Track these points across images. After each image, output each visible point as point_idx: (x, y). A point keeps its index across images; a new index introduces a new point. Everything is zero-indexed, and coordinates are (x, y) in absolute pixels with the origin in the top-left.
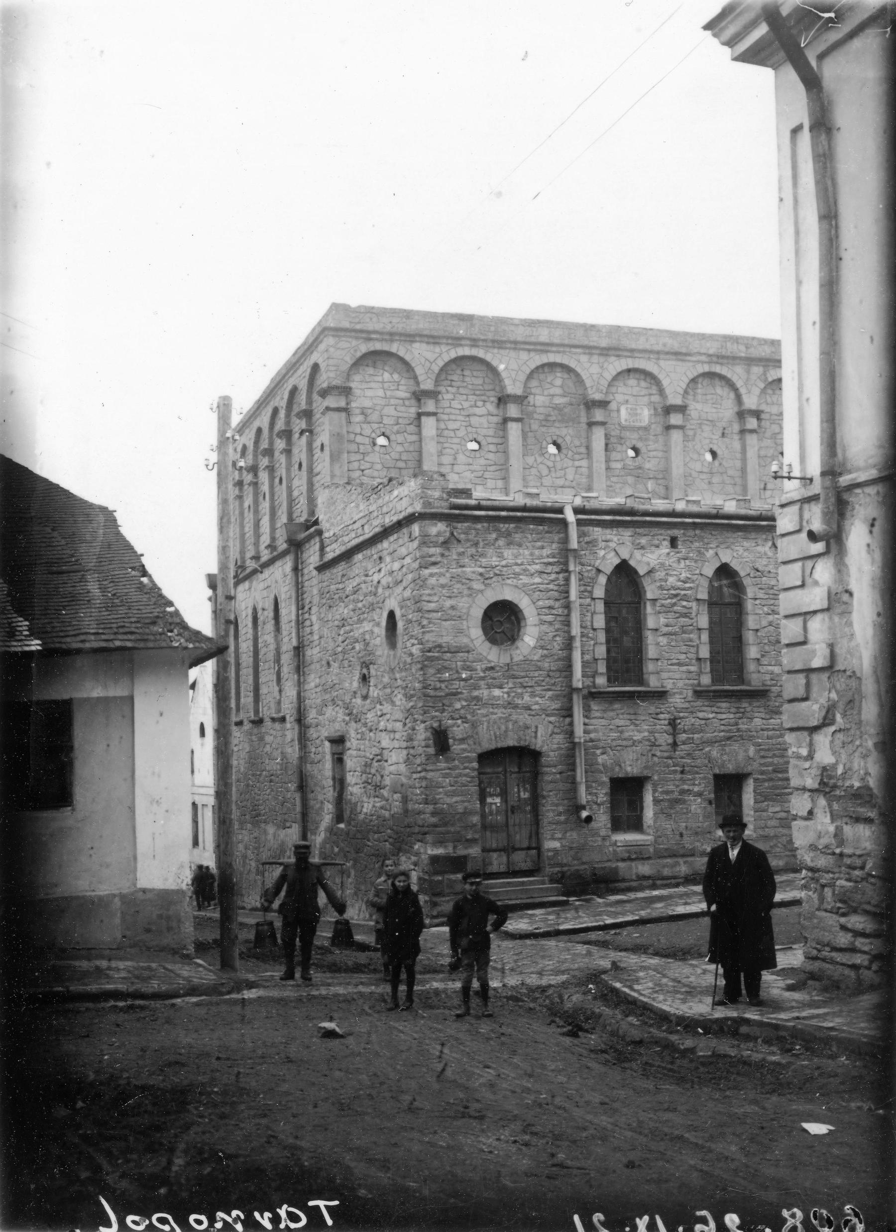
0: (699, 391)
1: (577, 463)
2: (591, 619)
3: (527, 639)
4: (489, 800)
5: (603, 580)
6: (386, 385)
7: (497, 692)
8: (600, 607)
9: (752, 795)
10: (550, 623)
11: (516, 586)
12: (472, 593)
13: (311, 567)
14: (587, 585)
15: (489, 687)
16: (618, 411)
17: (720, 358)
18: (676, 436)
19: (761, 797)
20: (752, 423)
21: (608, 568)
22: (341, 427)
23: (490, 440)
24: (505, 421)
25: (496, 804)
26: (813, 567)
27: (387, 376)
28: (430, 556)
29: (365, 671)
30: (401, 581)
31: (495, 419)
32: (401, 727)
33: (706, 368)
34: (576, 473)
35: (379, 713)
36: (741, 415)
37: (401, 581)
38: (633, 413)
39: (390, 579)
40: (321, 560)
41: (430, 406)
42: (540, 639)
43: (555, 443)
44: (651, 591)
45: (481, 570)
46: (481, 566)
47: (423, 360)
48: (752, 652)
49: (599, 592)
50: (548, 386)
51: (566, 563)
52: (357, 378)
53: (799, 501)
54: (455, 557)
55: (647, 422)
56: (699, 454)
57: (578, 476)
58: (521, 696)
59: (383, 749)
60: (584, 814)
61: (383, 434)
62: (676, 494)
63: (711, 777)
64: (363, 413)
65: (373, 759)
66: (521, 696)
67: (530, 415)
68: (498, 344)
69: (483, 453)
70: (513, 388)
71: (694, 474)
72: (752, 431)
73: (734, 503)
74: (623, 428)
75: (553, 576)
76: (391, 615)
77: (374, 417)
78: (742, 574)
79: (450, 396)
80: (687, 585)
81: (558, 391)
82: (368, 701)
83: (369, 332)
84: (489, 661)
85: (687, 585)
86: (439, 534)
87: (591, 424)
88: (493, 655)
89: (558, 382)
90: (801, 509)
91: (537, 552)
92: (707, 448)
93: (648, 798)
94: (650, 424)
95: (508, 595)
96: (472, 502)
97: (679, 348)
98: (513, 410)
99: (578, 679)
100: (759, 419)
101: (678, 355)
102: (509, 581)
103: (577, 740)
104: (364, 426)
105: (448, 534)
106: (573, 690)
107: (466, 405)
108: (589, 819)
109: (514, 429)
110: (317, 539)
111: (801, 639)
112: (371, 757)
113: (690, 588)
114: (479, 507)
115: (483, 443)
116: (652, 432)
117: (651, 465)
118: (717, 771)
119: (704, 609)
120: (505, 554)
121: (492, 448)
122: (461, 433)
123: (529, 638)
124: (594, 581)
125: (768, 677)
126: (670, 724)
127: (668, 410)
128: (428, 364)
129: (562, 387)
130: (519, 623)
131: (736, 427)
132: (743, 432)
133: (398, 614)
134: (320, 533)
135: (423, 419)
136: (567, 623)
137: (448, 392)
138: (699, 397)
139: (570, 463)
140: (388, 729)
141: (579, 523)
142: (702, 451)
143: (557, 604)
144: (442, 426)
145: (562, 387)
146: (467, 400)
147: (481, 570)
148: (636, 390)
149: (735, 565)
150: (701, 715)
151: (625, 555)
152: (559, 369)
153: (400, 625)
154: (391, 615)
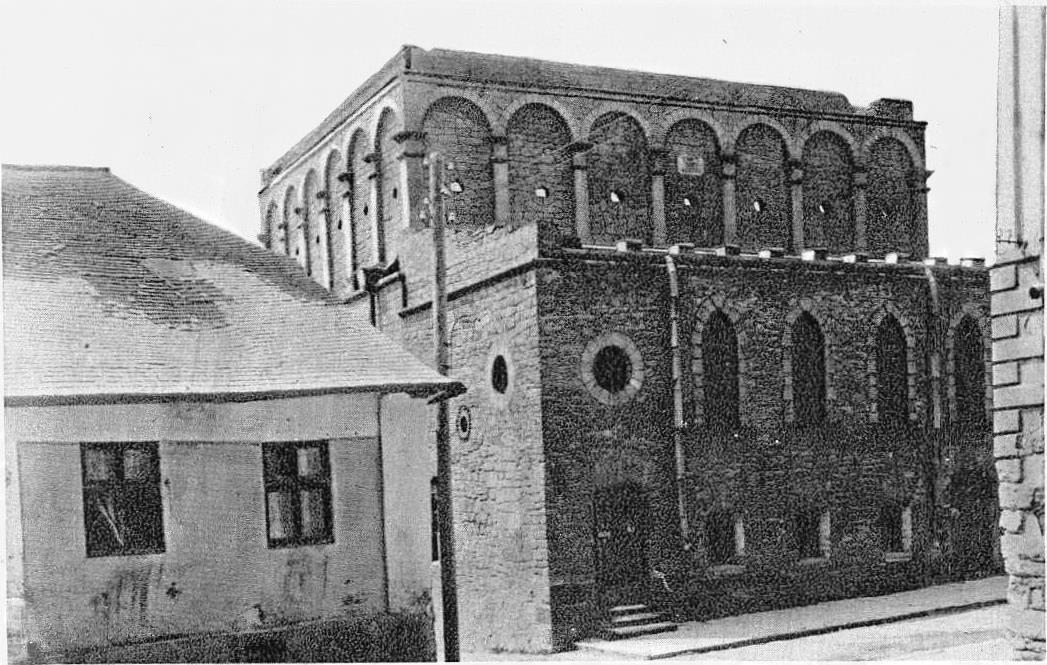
3: (633, 382)
4: (601, 535)
9: (829, 525)
12: (585, 341)
13: (806, 304)
16: (676, 162)
17: (768, 110)
19: (837, 529)
23: (560, 188)
24: (573, 168)
25: (607, 538)
26: (1027, 321)
29: (464, 414)
30: (514, 327)
31: (561, 167)
32: (513, 468)
33: (755, 119)
35: (484, 455)
37: (514, 327)
38: (691, 164)
39: (498, 325)
40: (405, 305)
41: (501, 152)
42: (644, 383)
43: (760, 202)
45: (591, 317)
53: (1013, 263)
55: (703, 171)
59: (489, 488)
61: (457, 181)
65: (476, 498)
69: (551, 198)
70: (499, 130)
72: (798, 182)
76: (500, 363)
82: (469, 443)
88: (603, 397)
91: (641, 300)
97: (733, 98)
111: (1016, 380)
112: (474, 496)
115: (552, 190)
121: (560, 196)
122: (531, 179)
133: (508, 360)
134: (402, 278)
135: (496, 166)
140: (496, 469)
147: (591, 317)
151: (719, 304)
153: (511, 371)
154: (500, 363)
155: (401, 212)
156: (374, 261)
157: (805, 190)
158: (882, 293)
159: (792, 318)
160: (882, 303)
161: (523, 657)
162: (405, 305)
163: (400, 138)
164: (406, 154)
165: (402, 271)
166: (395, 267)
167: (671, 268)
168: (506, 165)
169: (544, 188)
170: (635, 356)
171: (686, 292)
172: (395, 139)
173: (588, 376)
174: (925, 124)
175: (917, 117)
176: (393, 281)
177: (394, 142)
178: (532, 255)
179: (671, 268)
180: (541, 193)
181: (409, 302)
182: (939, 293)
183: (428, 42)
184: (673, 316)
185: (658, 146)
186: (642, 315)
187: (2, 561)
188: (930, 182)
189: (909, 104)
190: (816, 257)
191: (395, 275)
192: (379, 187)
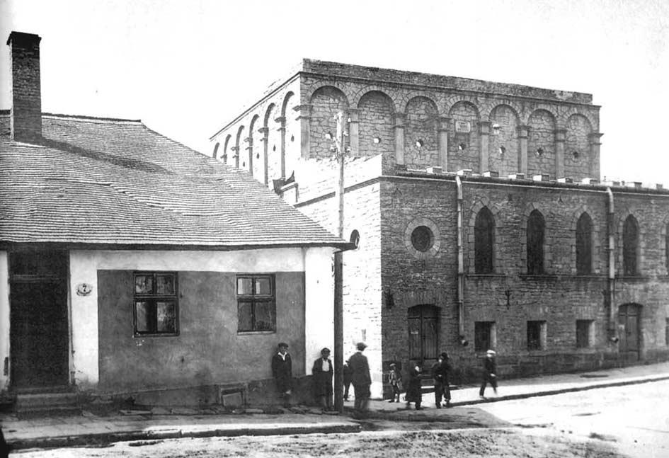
0: (497, 115)
1: (432, 152)
2: (466, 238)
5: (474, 216)
6: (331, 105)
7: (418, 275)
8: (472, 230)
10: (447, 239)
11: (430, 219)
13: (536, 206)
14: (466, 218)
15: (415, 272)
16: (455, 124)
17: (507, 97)
18: (485, 138)
19: (551, 334)
20: (525, 133)
21: (477, 210)
22: (307, 129)
23: (387, 138)
27: (331, 100)
28: (386, 201)
33: (502, 102)
34: (431, 158)
36: (519, 128)
38: (463, 126)
40: (297, 201)
44: (498, 224)
46: (411, 207)
47: (352, 92)
48: (548, 257)
49: (472, 223)
50: (417, 109)
51: (456, 207)
52: (316, 100)
54: (399, 202)
56: (496, 149)
57: (432, 160)
58: (430, 278)
60: (463, 341)
61: (329, 133)
62: (483, 168)
63: (525, 323)
64: (318, 121)
66: (430, 278)
67: (408, 125)
68: (394, 86)
71: (494, 160)
73: (489, 173)
74: (457, 134)
75: (449, 214)
77: (324, 123)
78: (544, 215)
79: (365, 113)
80: (517, 221)
81: (423, 112)
83: (323, 75)
84: (415, 259)
85: (517, 221)
86: (390, 190)
87: (439, 131)
88: (418, 255)
89: (423, 107)
90: (284, 175)
91: (441, 200)
92: (500, 146)
93: (494, 333)
94: (471, 132)
95: (426, 223)
96: (407, 173)
98: (399, 122)
99: (461, 269)
100: (529, 132)
101: (488, 95)
102: (426, 216)
103: (460, 302)
104: (319, 128)
105: (395, 189)
106: (458, 275)
107: (374, 118)
108: (466, 344)
109: (400, 133)
110: (294, 189)
113: (518, 223)
114: (411, 175)
116: (472, 136)
117: (472, 154)
118: (529, 320)
119: (524, 233)
120: (425, 202)
123: (436, 246)
124: (470, 217)
125: (556, 270)
126: (506, 294)
127: (480, 124)
128: (354, 95)
129: (424, 110)
130: (429, 238)
131: (515, 135)
132: (520, 137)
134: (296, 186)
135: (397, 129)
136: (457, 240)
137: (364, 110)
138: (497, 118)
139: (428, 152)
141: (463, 185)
142: (497, 148)
143: (451, 229)
144: (361, 129)
145: (424, 110)
146: (374, 115)
148: (464, 113)
149: (540, 210)
150: (522, 289)
151: (486, 204)
152: (546, 114)
155: (294, 148)
156: (278, 177)
157: (529, 142)
158: (581, 201)
159: (528, 213)
160: (582, 206)
161: (375, 438)
162: (297, 201)
163: (296, 109)
164: (300, 117)
165: (296, 182)
166: (292, 180)
167: (459, 183)
168: (357, 125)
169: (378, 138)
170: (434, 229)
171: (467, 197)
172: (293, 109)
173: (408, 243)
174: (600, 107)
175: (595, 102)
176: (292, 187)
177: (293, 111)
178: (379, 173)
179: (459, 183)
180: (376, 141)
181: (298, 200)
182: (614, 200)
183: (314, 57)
184: (459, 210)
185: (444, 115)
186: (441, 209)
187: (21, 456)
188: (602, 140)
189: (591, 96)
190: (566, 182)
191: (292, 184)
192: (283, 136)
